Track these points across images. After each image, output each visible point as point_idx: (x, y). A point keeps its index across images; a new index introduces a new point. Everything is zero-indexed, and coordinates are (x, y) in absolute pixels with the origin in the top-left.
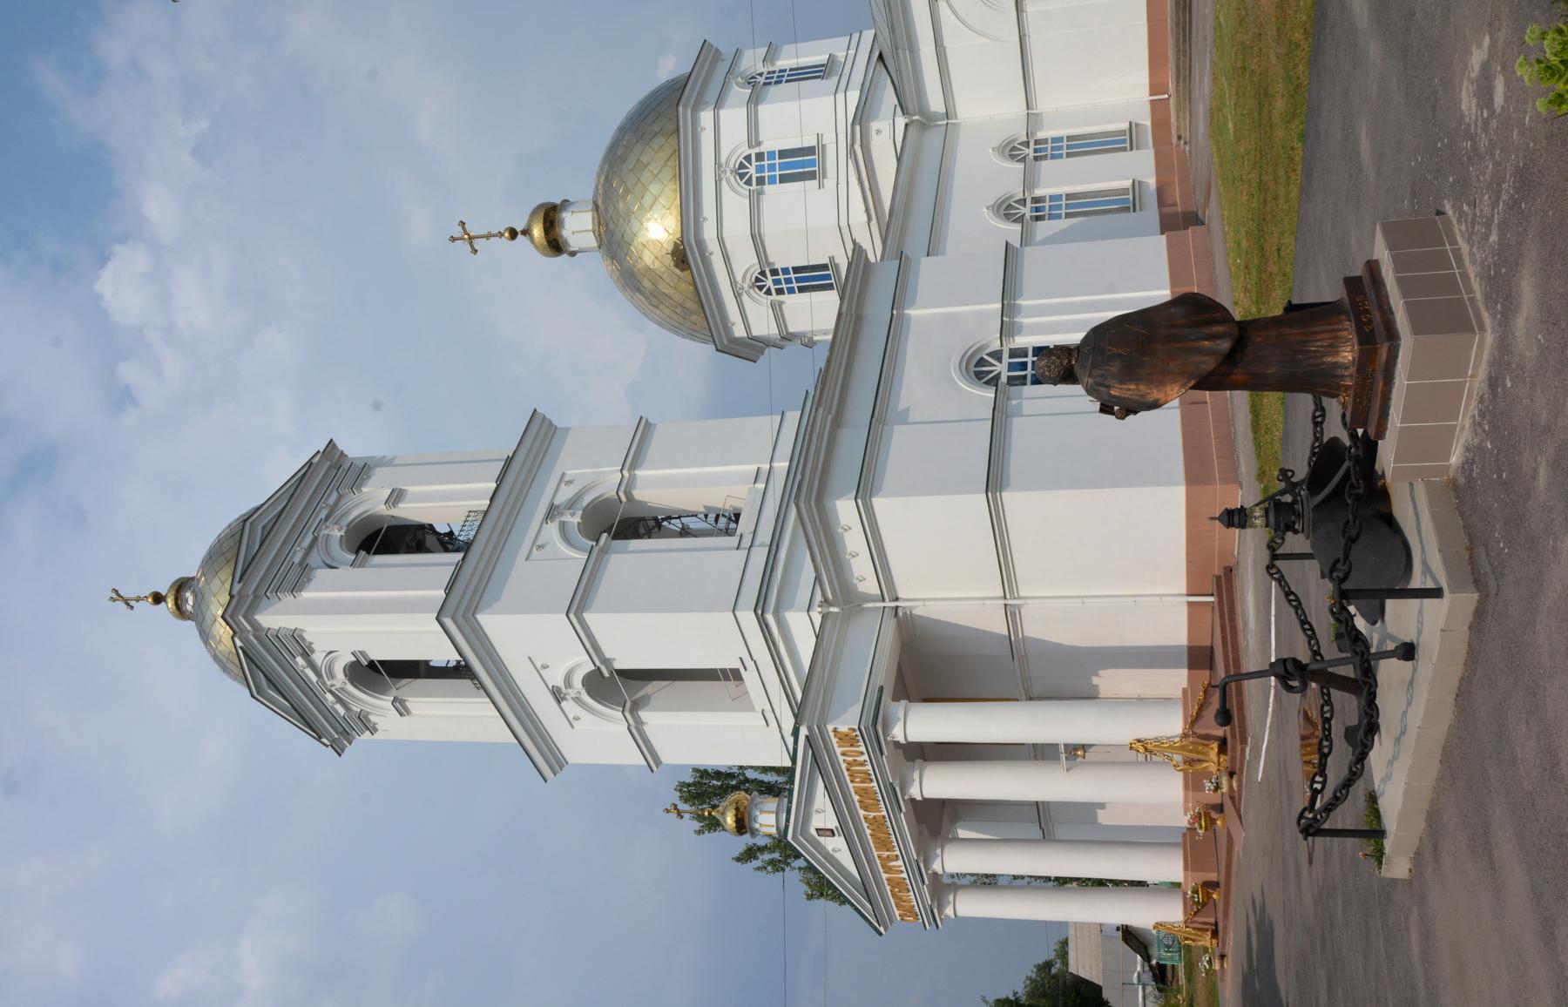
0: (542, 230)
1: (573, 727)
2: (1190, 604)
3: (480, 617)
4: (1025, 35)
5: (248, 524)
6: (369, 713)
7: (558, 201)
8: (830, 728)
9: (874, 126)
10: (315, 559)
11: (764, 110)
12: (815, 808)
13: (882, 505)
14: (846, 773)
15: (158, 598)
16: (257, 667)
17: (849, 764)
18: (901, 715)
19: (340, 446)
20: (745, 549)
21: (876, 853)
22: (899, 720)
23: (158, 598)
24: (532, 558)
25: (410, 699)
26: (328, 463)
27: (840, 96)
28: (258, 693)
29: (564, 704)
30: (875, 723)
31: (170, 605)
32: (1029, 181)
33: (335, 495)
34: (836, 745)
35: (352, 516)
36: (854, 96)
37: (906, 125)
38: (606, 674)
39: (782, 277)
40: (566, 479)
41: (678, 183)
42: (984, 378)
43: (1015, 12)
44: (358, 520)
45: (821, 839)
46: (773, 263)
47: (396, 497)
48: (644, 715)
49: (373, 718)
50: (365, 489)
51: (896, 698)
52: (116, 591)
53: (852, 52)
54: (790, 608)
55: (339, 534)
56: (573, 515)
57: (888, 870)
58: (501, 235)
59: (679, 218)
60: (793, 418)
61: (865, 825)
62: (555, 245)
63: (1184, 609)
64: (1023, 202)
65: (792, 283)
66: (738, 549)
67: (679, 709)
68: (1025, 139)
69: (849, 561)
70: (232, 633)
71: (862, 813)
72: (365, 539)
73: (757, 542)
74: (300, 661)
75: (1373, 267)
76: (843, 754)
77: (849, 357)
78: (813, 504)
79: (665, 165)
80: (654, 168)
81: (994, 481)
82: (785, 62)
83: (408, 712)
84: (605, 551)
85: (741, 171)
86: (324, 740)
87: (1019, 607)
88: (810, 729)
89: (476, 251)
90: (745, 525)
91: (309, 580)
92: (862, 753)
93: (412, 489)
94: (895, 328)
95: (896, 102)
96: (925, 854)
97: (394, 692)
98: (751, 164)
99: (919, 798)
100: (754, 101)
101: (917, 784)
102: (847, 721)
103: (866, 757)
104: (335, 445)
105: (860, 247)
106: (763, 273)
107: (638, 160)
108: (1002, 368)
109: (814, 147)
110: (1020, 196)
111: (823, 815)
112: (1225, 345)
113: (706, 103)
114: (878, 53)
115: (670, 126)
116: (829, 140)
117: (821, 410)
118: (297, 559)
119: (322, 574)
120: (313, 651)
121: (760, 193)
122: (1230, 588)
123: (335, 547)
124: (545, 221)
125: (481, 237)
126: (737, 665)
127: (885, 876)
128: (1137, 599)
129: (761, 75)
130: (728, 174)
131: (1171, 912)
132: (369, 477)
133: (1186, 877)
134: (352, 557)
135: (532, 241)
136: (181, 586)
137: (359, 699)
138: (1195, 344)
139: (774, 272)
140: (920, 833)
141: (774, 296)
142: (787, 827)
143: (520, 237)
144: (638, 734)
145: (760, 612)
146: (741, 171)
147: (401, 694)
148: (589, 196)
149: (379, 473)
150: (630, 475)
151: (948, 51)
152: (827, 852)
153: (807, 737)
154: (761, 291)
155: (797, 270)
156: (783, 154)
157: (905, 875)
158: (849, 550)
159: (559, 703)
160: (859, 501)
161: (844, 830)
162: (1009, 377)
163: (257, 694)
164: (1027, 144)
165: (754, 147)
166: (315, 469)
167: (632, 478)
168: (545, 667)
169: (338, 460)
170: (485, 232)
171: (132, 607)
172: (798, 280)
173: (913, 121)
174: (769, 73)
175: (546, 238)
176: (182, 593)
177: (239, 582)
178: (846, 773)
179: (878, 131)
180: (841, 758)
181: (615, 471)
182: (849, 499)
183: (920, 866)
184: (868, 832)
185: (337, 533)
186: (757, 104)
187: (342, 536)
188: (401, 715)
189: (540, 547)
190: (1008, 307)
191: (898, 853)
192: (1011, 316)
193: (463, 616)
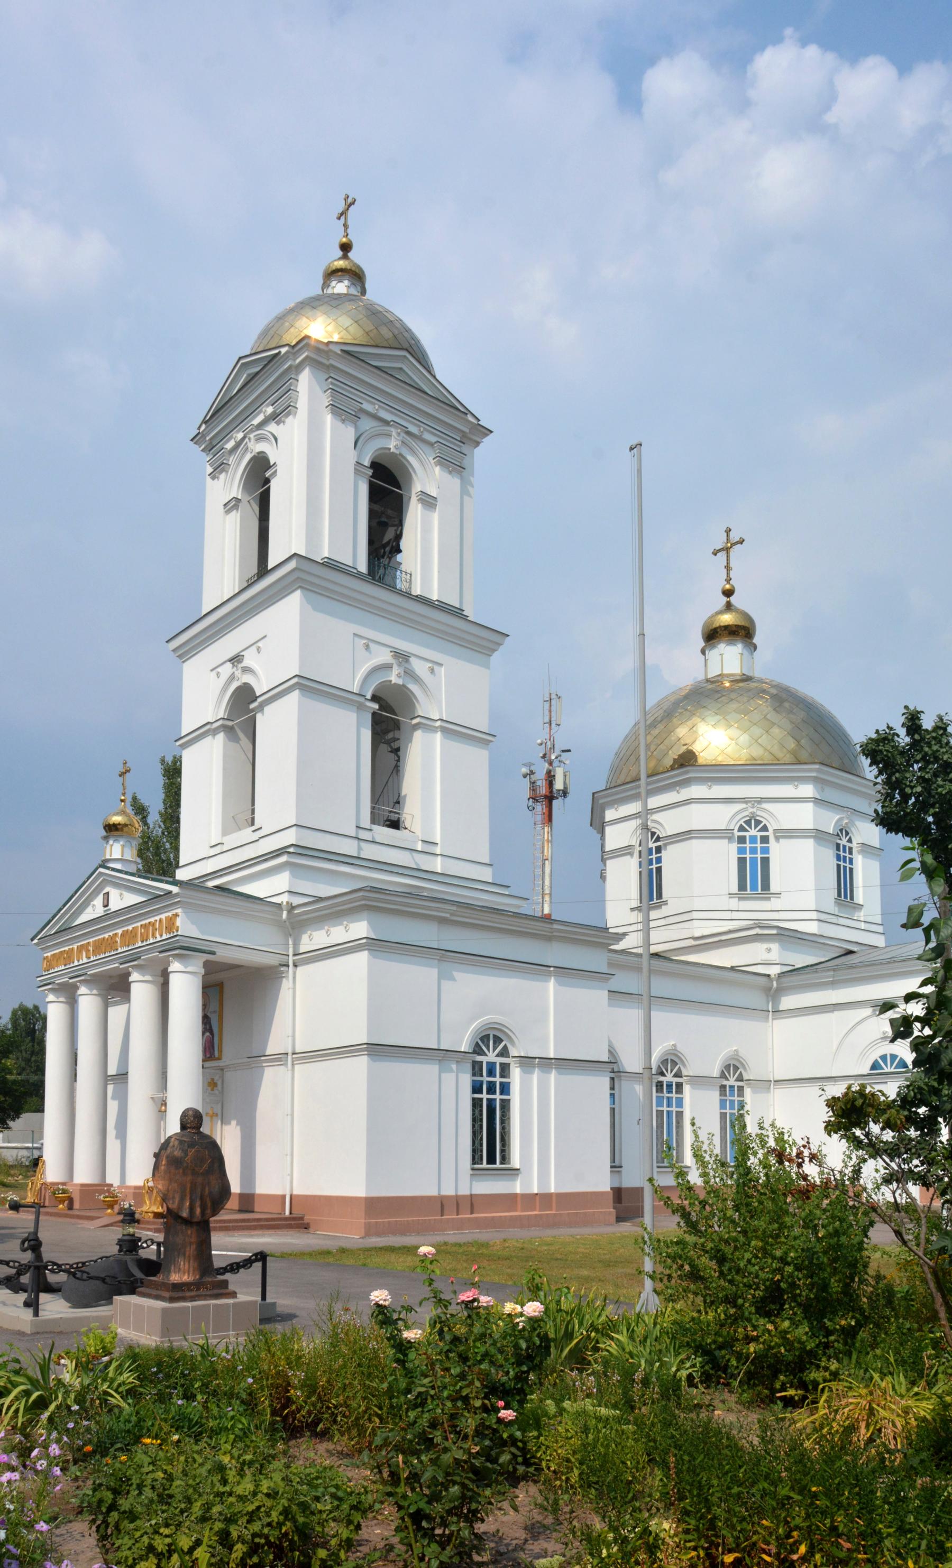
0: (726, 624)
1: (212, 670)
2: (284, 1197)
3: (298, 593)
4: (835, 1081)
5: (404, 353)
6: (227, 472)
7: (756, 640)
8: (179, 911)
9: (775, 947)
10: (367, 424)
11: (809, 844)
12: (124, 893)
13: (362, 958)
14: (147, 921)
15: (346, 248)
16: (265, 366)
17: (153, 924)
18: (189, 969)
19: (487, 441)
20: (357, 833)
21: (91, 940)
22: (186, 967)
23: (346, 248)
24: (357, 639)
25: (239, 514)
26: (467, 430)
27: (814, 915)
28: (243, 364)
29: (229, 665)
30: (186, 949)
31: (336, 263)
32: (699, 1081)
33: (433, 439)
34: (167, 915)
35: (410, 458)
36: (812, 928)
37: (769, 976)
38: (252, 706)
39: (654, 856)
40: (436, 668)
41: (748, 762)
42: (483, 1042)
43: (856, 1073)
44: (406, 463)
45: (100, 897)
46: (666, 849)
47: (429, 501)
48: (221, 736)
49: (223, 476)
50: (437, 469)
51: (207, 964)
52: (353, 203)
53: (863, 926)
54: (293, 875)
55: (391, 447)
56: (399, 676)
57: (80, 949)
58: (728, 580)
59: (714, 763)
60: (486, 874)
61: (111, 934)
62: (713, 635)
63: (279, 1192)
64: (678, 1075)
65: (657, 863)
66: (358, 827)
67: (225, 769)
68: (745, 1077)
69: (323, 928)
70: (293, 344)
71: (120, 931)
72: (390, 471)
73: (363, 844)
74: (270, 410)
75: (233, 1295)
76: (161, 920)
77: (504, 929)
78: (363, 902)
79: (766, 749)
80: (764, 740)
81: (376, 1050)
82: (859, 862)
83: (228, 512)
84: (360, 707)
85: (753, 822)
86: (204, 427)
87: (286, 1064)
88: (177, 895)
89: (715, 554)
90: (383, 833)
91: (343, 421)
92: (161, 936)
93: (435, 517)
94: (539, 969)
95: (797, 966)
96: (93, 981)
97: (245, 498)
98: (759, 831)
99: (131, 979)
100: (819, 835)
101: (141, 978)
102: (186, 926)
103: (159, 939)
104: (487, 435)
105: (621, 939)
106: (658, 839)
107: (774, 724)
108: (491, 1056)
109: (769, 890)
110: (684, 1073)
111: (120, 900)
112: (185, 1214)
113: (823, 790)
114: (855, 949)
115: (804, 755)
116: (774, 904)
117: (454, 908)
118: (367, 406)
119: (349, 433)
120: (278, 423)
121: (730, 839)
122: (290, 1227)
123: (379, 443)
124: (737, 626)
125: (728, 560)
126: (257, 824)
127: (75, 946)
128: (289, 1158)
129: (850, 841)
130: (751, 810)
131: (52, 1172)
132: (450, 472)
133: (76, 1185)
134: (367, 462)
135: (721, 612)
136: (356, 276)
137: (239, 464)
138: (188, 1198)
139: (659, 850)
140: (110, 977)
141: (638, 849)
142: (108, 868)
143: (725, 599)
144: (204, 732)
145: (291, 850)
146: (753, 822)
147: (244, 505)
148: (757, 673)
149: (454, 483)
150: (437, 728)
151: (830, 1014)
152: (92, 900)
153: (171, 892)
154: (745, 822)
155: (659, 870)
156: (766, 862)
157: (76, 963)
158: (332, 929)
159: (230, 660)
160: (364, 941)
161: (107, 916)
162: (482, 1062)
163: (242, 363)
164: (740, 1079)
165: (774, 834)
166: (462, 418)
167: (433, 730)
168: (259, 650)
169: (470, 439)
170: (732, 565)
171: (339, 218)
172: (754, 860)
173: (772, 982)
174: (851, 849)
175: (720, 627)
176: (347, 277)
177: (342, 350)
178: (147, 921)
179: (769, 950)
180: (157, 918)
181: (441, 713)
182: (368, 932)
183: (80, 975)
184: (106, 936)
185: (392, 444)
186: (814, 837)
187: (390, 449)
188: (225, 505)
189: (367, 647)
190: (546, 1063)
191: (92, 959)
192: (539, 1065)
193: (298, 578)
